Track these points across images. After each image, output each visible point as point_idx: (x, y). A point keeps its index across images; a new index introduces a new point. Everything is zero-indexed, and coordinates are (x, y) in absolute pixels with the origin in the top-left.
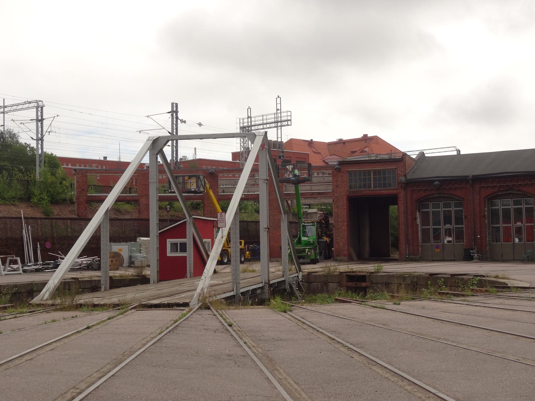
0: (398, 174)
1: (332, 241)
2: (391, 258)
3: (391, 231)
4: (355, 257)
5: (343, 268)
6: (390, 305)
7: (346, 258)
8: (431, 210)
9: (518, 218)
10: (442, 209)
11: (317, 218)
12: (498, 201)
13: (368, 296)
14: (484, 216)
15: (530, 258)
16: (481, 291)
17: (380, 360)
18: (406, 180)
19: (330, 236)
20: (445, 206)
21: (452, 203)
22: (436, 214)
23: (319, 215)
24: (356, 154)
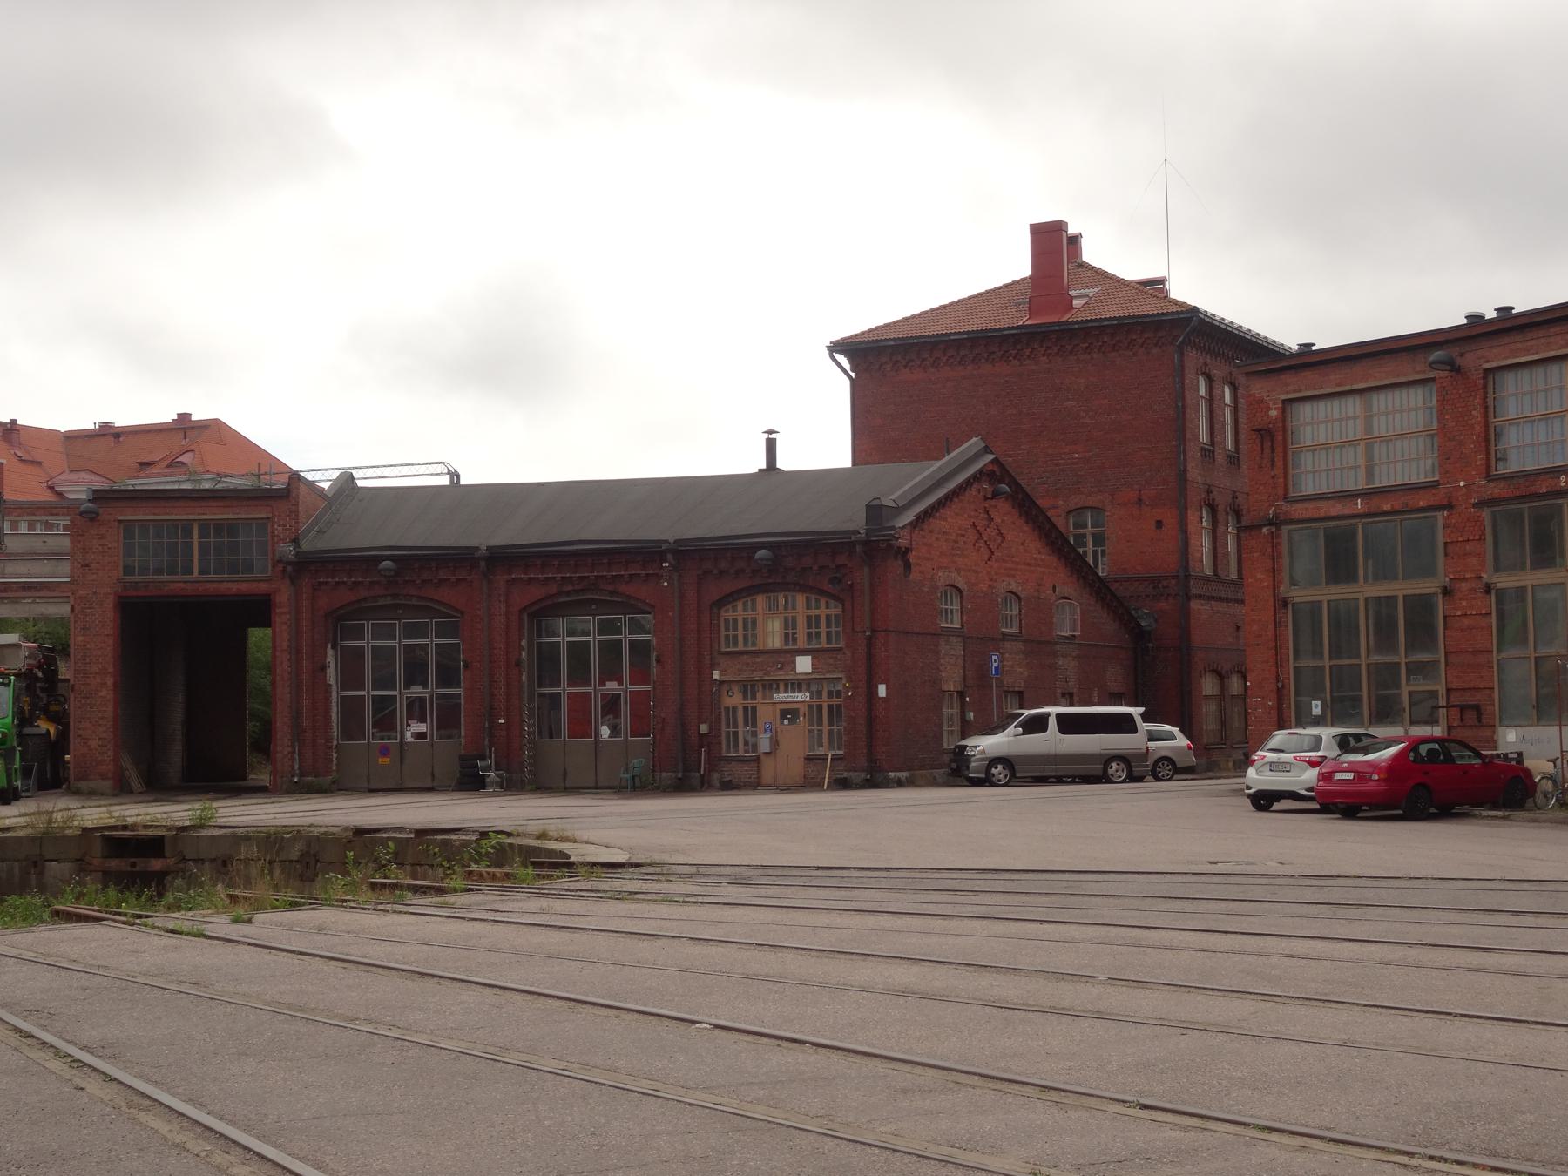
0: (273, 536)
1: (64, 735)
2: (251, 783)
3: (251, 704)
4: (136, 784)
5: (95, 814)
6: (222, 926)
7: (107, 785)
8: (367, 643)
9: (611, 671)
10: (400, 642)
11: (17, 663)
12: (560, 623)
13: (170, 897)
14: (518, 664)
15: (638, 784)
16: (493, 877)
17: (168, 1091)
18: (297, 554)
19: (60, 718)
20: (411, 631)
21: (431, 624)
22: (384, 657)
23: (25, 653)
24: (154, 470)
